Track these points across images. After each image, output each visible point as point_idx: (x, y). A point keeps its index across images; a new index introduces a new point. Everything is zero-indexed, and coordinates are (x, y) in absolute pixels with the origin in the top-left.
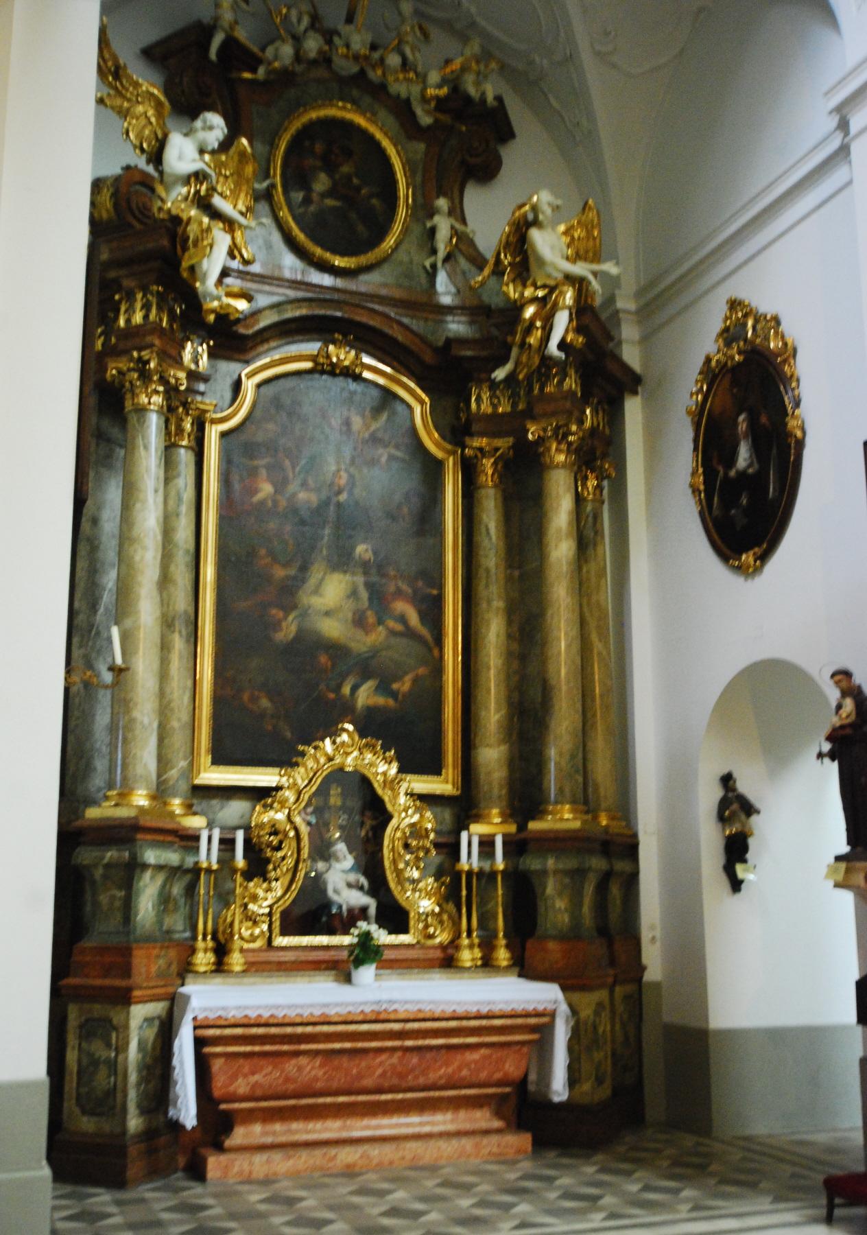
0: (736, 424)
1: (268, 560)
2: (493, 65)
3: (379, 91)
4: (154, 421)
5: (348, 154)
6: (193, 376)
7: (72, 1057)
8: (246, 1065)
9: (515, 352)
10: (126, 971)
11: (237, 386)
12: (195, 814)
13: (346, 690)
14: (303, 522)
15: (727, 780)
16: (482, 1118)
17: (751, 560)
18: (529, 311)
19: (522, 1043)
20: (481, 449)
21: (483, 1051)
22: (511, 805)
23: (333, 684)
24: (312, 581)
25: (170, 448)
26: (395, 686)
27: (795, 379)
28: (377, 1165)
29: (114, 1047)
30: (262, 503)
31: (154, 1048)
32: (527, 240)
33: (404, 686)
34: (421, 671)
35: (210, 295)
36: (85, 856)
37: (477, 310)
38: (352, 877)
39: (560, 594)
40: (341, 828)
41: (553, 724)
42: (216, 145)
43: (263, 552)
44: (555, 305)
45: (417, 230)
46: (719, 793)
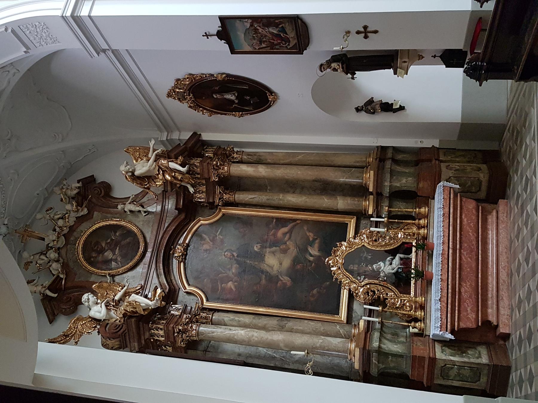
0: (217, 98)
1: (258, 286)
2: (65, 182)
3: (72, 229)
4: (202, 329)
5: (97, 243)
6: (184, 311)
7: (456, 384)
8: (463, 314)
9: (183, 184)
10: (422, 358)
11: (188, 293)
12: (359, 324)
13: (311, 259)
14: (244, 271)
15: (358, 110)
16: (492, 219)
17: (272, 97)
18: (168, 177)
19: (461, 201)
20: (220, 199)
21: (463, 217)
22: (362, 196)
23: (308, 264)
24: (268, 269)
25: (212, 323)
26: (311, 239)
27: (201, 75)
28: (508, 263)
29: (453, 366)
30: (235, 287)
31: (455, 350)
32: (139, 176)
33: (311, 235)
34: (305, 228)
35: (155, 303)
36: (374, 371)
37: (164, 195)
38: (387, 263)
39: (279, 172)
40: (367, 266)
41: (331, 179)
42: (95, 297)
43: (255, 288)
44: (166, 167)
45: (130, 217)
46: (363, 113)
